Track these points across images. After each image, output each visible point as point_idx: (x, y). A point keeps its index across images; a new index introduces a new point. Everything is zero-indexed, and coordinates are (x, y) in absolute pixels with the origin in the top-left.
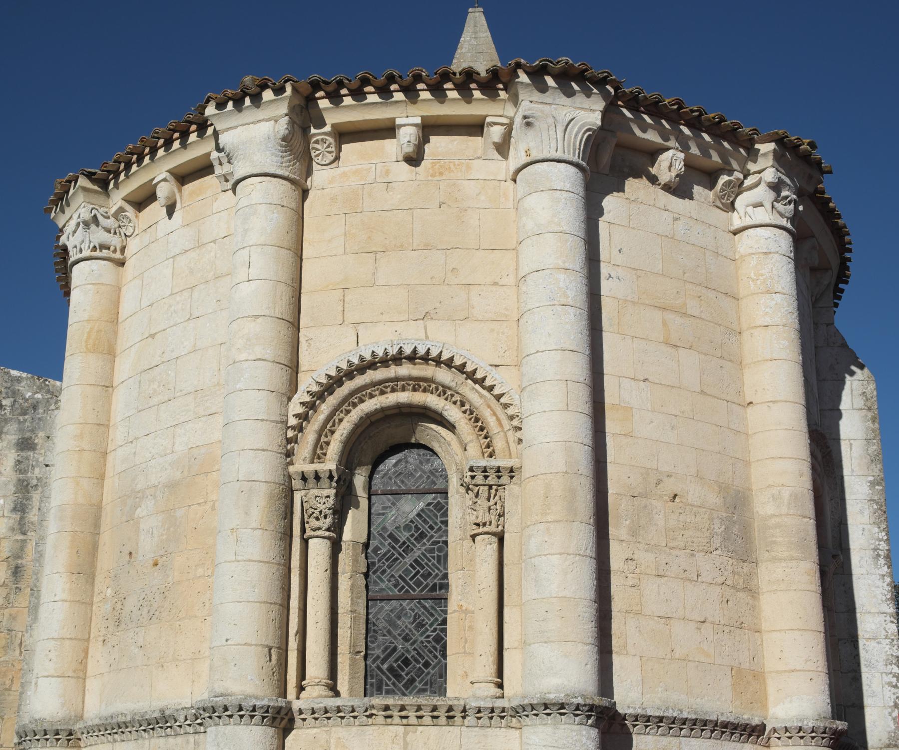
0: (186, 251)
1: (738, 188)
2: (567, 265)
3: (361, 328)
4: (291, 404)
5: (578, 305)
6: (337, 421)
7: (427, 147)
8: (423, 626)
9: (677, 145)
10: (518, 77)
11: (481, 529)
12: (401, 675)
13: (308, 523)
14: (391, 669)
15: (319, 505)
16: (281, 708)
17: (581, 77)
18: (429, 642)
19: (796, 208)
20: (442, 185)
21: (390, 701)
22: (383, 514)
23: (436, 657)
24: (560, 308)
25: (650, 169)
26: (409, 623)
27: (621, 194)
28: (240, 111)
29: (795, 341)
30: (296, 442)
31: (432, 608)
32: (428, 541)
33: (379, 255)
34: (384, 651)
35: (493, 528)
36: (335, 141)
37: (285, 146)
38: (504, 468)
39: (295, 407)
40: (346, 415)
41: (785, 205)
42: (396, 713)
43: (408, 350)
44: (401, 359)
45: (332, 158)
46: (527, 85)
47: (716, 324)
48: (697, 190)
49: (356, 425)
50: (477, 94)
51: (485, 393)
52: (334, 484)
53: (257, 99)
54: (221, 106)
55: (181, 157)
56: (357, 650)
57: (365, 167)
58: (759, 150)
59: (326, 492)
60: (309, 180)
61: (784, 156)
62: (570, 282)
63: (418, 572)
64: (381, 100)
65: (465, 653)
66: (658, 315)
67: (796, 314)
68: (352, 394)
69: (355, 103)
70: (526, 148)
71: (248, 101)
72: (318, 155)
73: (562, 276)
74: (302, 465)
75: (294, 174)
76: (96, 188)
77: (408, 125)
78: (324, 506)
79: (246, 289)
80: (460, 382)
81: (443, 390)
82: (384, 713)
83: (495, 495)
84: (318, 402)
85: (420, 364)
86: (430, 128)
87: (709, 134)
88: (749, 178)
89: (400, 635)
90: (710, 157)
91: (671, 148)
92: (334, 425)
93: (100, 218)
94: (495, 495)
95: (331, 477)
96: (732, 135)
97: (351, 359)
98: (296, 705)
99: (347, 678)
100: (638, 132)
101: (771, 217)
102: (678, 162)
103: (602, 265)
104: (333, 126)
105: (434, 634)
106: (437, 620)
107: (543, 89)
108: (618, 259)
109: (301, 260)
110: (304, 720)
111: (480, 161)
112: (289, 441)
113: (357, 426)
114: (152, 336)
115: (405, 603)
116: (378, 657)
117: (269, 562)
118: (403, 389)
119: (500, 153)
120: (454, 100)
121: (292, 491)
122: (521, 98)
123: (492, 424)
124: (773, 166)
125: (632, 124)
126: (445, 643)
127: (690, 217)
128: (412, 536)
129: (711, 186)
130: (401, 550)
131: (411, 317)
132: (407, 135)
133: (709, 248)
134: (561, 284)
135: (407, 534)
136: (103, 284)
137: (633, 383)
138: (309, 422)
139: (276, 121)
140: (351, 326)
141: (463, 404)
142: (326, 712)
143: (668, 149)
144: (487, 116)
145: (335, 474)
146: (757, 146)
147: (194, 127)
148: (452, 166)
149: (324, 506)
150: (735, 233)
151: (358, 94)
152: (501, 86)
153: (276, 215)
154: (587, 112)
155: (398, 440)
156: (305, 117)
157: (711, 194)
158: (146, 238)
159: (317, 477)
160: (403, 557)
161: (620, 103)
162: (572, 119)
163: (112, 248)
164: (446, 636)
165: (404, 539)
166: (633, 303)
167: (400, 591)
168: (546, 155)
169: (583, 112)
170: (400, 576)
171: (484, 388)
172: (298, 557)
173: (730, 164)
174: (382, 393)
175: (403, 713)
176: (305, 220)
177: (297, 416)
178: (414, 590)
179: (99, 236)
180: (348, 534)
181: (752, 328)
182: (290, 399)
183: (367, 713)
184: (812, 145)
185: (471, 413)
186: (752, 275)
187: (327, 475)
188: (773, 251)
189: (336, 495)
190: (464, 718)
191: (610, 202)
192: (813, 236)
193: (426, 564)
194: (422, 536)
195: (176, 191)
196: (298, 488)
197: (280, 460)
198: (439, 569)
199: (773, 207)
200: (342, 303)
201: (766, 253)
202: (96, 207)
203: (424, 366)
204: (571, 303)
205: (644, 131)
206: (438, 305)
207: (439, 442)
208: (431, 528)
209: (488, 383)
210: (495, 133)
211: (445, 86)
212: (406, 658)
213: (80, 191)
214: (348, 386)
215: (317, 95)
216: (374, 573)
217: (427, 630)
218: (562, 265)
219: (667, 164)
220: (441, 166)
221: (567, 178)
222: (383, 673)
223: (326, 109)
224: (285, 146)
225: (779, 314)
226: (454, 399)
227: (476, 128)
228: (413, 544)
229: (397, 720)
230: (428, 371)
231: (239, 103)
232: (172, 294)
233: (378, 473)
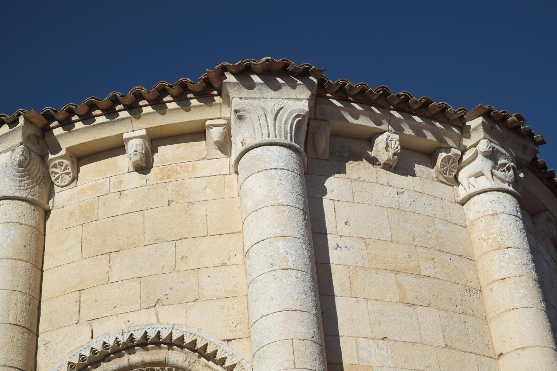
1: (459, 163)
2: (285, 233)
5: (299, 268)
7: (155, 156)
9: (390, 128)
10: (226, 78)
17: (285, 72)
19: (516, 175)
20: (170, 186)
24: (280, 272)
25: (370, 153)
27: (343, 175)
29: (535, 289)
33: (112, 256)
36: (72, 163)
37: (22, 171)
41: (504, 171)
43: (138, 336)
45: (70, 179)
46: (235, 84)
47: (454, 283)
48: (419, 168)
50: (194, 102)
51: (218, 367)
57: (100, 181)
58: (470, 126)
60: (51, 201)
61: (493, 128)
62: (290, 248)
64: (108, 120)
66: (391, 278)
67: (532, 265)
69: (85, 126)
70: (241, 139)
72: (57, 179)
73: (281, 243)
75: (34, 195)
77: (134, 138)
80: (192, 361)
85: (152, 349)
86: (156, 140)
87: (420, 116)
88: (467, 153)
90: (425, 137)
91: (385, 131)
96: (441, 115)
97: (83, 353)
100: (350, 119)
101: (492, 182)
102: (393, 142)
103: (329, 237)
104: (68, 149)
107: (251, 86)
108: (346, 231)
109: (42, 271)
111: (205, 161)
119: (222, 152)
120: (174, 110)
122: (231, 96)
124: (485, 138)
125: (343, 112)
127: (415, 191)
129: (432, 164)
131: (143, 306)
132: (135, 147)
133: (438, 216)
134: (281, 250)
137: (371, 342)
139: (13, 151)
140: (86, 323)
143: (382, 132)
144: (206, 120)
146: (468, 124)
148: (179, 168)
150: (462, 203)
151: (87, 118)
152: (215, 92)
153: (13, 232)
154: (296, 100)
156: (40, 144)
157: (433, 172)
161: (328, 95)
162: (281, 109)
166: (364, 268)
168: (259, 140)
169: (290, 102)
171: (216, 363)
173: (445, 142)
176: (46, 237)
181: (491, 283)
184: (519, 117)
186: (483, 236)
188: (499, 211)
191: (333, 183)
192: (547, 210)
199: (493, 174)
200: (78, 304)
201: (492, 215)
203: (157, 351)
204: (292, 266)
205: (357, 118)
206: (169, 291)
209: (218, 356)
210: (215, 134)
211: (165, 100)
215: (52, 125)
218: (280, 233)
219: (383, 145)
220: (169, 170)
221: (281, 157)
223: (61, 135)
224: (22, 171)
225: (515, 266)
227: (198, 133)
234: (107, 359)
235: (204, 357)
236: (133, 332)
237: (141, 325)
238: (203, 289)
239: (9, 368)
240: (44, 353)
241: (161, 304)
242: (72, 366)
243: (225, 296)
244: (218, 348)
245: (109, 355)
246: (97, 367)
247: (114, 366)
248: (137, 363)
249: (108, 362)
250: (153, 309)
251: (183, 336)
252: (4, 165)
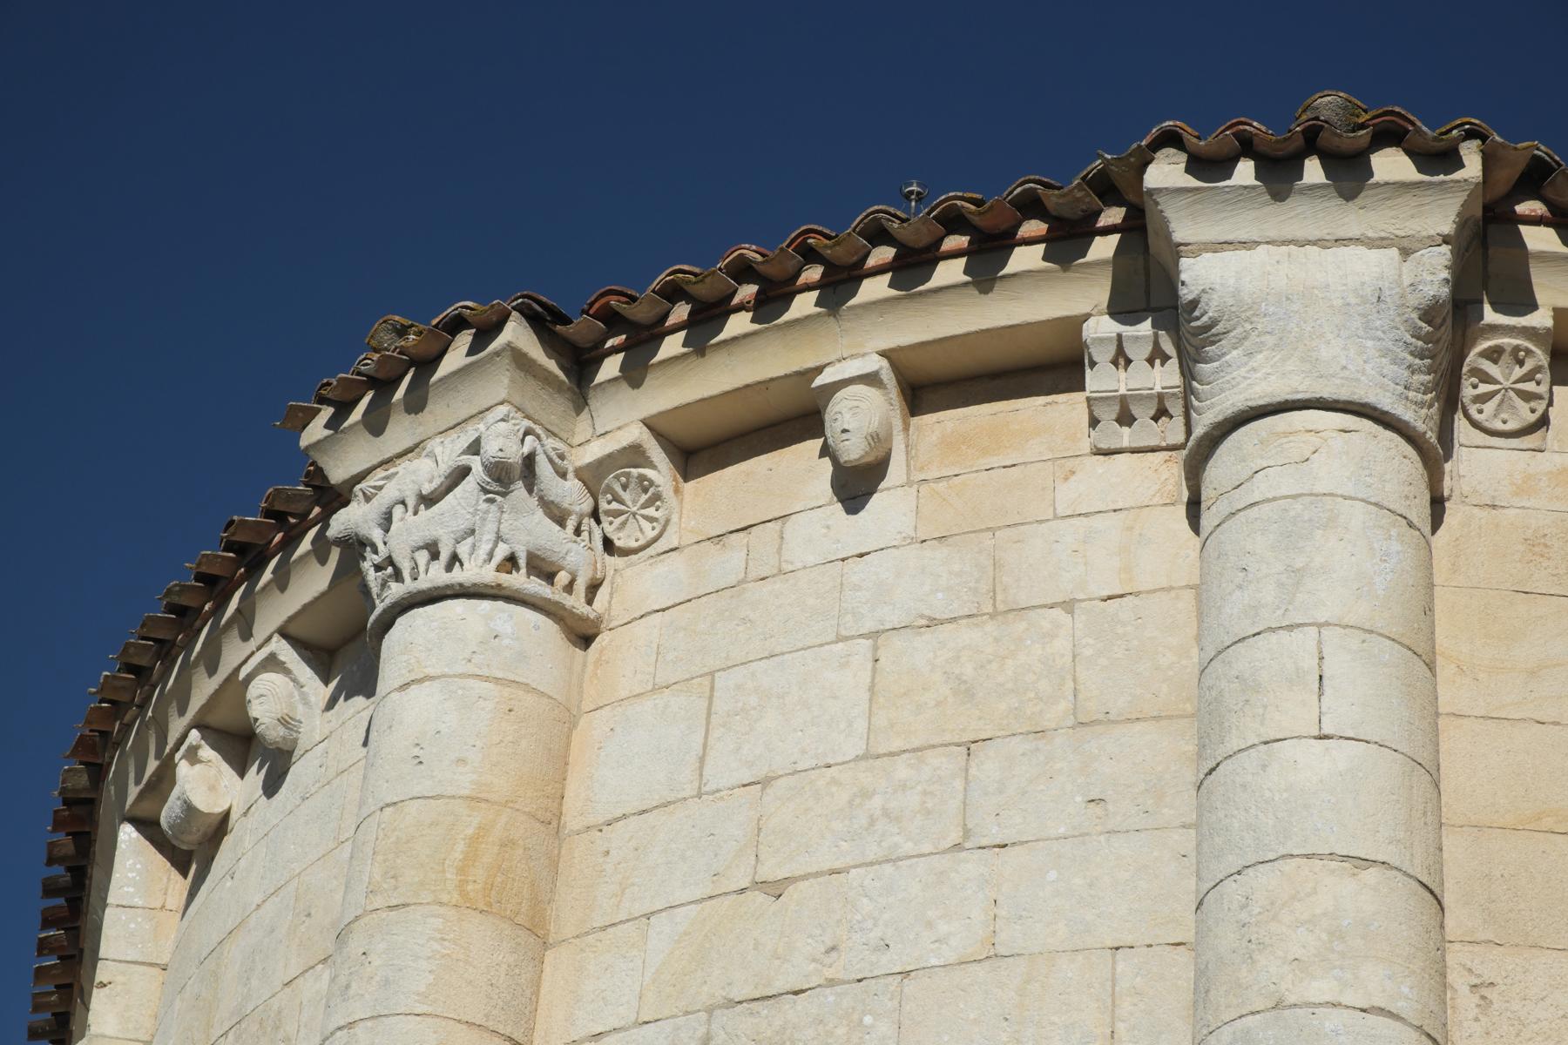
0: (932, 623)
28: (1279, 196)
45: (1533, 418)
53: (1349, 171)
54: (1209, 166)
55: (955, 312)
71: (1313, 171)
72: (1483, 398)
76: (552, 365)
79: (1312, 765)
93: (543, 468)
114: (776, 889)
136: (527, 687)
139: (1406, 253)
147: (814, 273)
153: (1396, 546)
158: (729, 562)
163: (562, 578)
179: (527, 527)
195: (897, 423)
202: (539, 430)
213: (505, 361)
224: (1426, 339)
231: (1279, 172)
232: (866, 756)
252: (1369, 290)
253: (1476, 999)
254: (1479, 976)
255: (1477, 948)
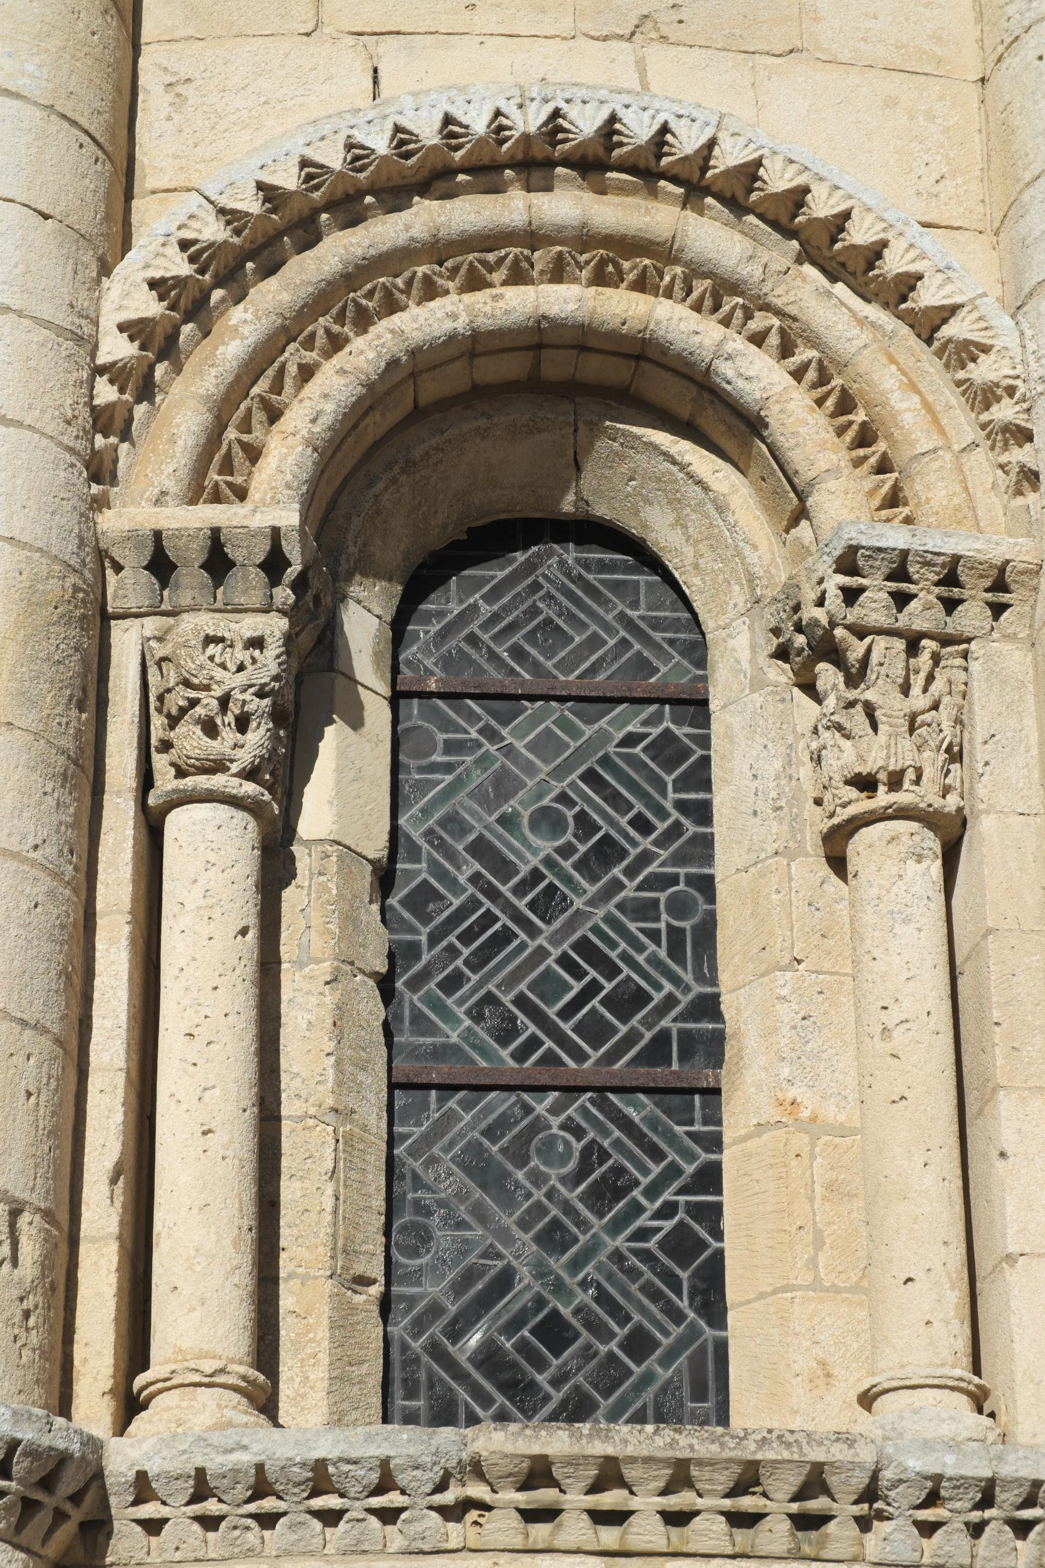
3: (390, 56)
4: (114, 287)
6: (292, 369)
8: (619, 1193)
11: (883, 798)
12: (533, 1385)
13: (166, 746)
14: (489, 1358)
15: (218, 673)
16: (63, 1459)
18: (646, 1256)
21: (556, 1442)
22: (448, 768)
23: (678, 1317)
26: (563, 1180)
30: (126, 435)
31: (653, 1123)
32: (631, 872)
34: (460, 1286)
35: (923, 794)
38: (974, 565)
39: (126, 295)
40: (328, 355)
42: (575, 1499)
44: (550, 164)
49: (370, 386)
52: (284, 595)
56: (359, 1268)
59: (249, 625)
63: (593, 988)
65: (816, 1285)
68: (355, 275)
74: (152, 498)
78: (241, 678)
81: (720, 293)
82: (522, 1498)
83: (930, 678)
84: (217, 294)
85: (622, 189)
89: (524, 1225)
92: (277, 387)
94: (930, 678)
95: (274, 565)
97: (360, 137)
98: (123, 1458)
99: (320, 1374)
105: (668, 1225)
106: (674, 1171)
110: (153, 1527)
112: (103, 420)
113: (373, 399)
115: (542, 1105)
116: (435, 1310)
117: (15, 856)
118: (558, 274)
121: (105, 618)
123: (908, 419)
126: (718, 1259)
128: (566, 851)
130: (522, 904)
131: (586, 26)
135: (546, 846)
138: (178, 369)
140: (351, 40)
141: (786, 350)
142: (261, 1488)
145: (293, 551)
149: (241, 678)
155: (506, 498)
159: (218, 562)
160: (533, 931)
164: (718, 1234)
165: (535, 861)
167: (521, 1055)
170: (521, 1001)
172: (128, 855)
174: (475, 283)
175: (610, 1499)
177: (132, 329)
178: (580, 1056)
180: (318, 814)
182: (105, 269)
183: (448, 1497)
185: (823, 379)
187: (261, 551)
189: (289, 639)
190: (864, 1524)
193: (625, 957)
194: (607, 852)
196: (132, 602)
197: (67, 477)
198: (676, 980)
207: (676, 502)
208: (643, 825)
212: (555, 1314)
214: (338, 249)
216: (414, 984)
217: (639, 1209)
222: (460, 1376)
226: (753, 325)
228: (568, 880)
229: (575, 1528)
230: (656, 216)
233: (427, 618)
234: (441, 186)
235: (814, 263)
236: (562, 105)
237: (594, 87)
238: (817, 20)
239: (66, 125)
240: (169, 118)
241: (654, 35)
242: (357, 158)
243: (899, 63)
244: (889, 236)
245: (448, 172)
246: (399, 209)
247: (472, 217)
248: (561, 228)
249: (441, 198)
250: (625, 45)
251: (758, 163)
253: (170, 98)
254: (175, 74)
255: (174, 46)
